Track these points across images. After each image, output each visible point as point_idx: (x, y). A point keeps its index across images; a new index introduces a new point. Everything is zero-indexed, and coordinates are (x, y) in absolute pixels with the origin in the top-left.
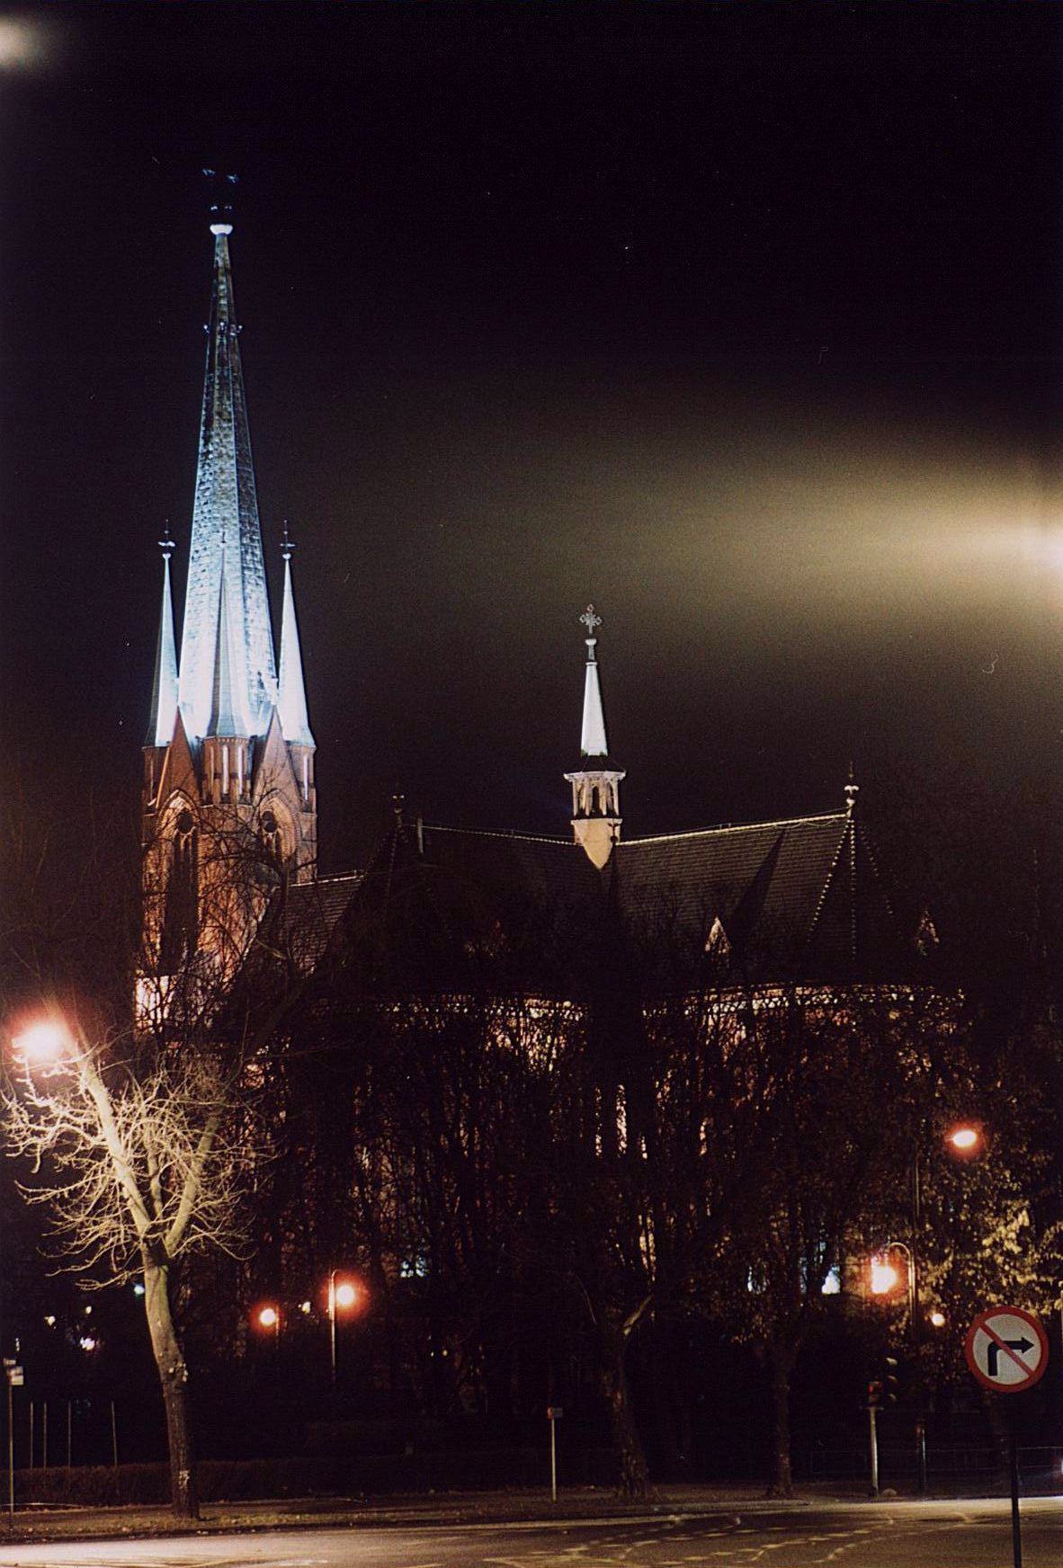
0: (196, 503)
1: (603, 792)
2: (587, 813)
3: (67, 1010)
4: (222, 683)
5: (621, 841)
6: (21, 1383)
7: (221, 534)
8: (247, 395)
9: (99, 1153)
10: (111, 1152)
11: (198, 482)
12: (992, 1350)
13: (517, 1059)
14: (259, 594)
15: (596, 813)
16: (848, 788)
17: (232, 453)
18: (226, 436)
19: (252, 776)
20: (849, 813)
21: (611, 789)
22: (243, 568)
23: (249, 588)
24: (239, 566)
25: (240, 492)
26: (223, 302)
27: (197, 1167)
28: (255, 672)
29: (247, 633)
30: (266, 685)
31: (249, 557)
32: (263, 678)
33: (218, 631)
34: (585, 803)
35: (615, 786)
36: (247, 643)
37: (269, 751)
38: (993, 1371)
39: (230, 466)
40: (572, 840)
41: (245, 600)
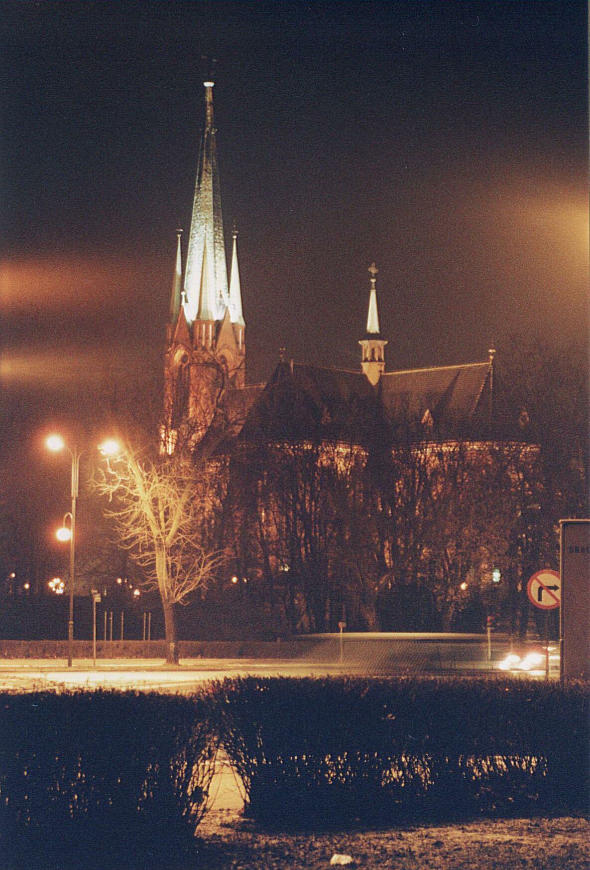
0: (194, 211)
1: (376, 350)
2: (369, 360)
3: (123, 435)
4: (203, 295)
6: (100, 601)
7: (204, 226)
8: (218, 160)
9: (136, 499)
11: (195, 202)
12: (540, 589)
13: (331, 470)
14: (221, 254)
15: (373, 360)
16: (491, 351)
17: (211, 189)
18: (208, 181)
19: (216, 338)
20: (491, 363)
21: (380, 349)
22: (215, 242)
23: (217, 252)
24: (212, 241)
25: (214, 207)
26: (209, 118)
27: (180, 507)
28: (218, 290)
29: (215, 273)
30: (223, 296)
31: (217, 237)
32: (222, 293)
33: (202, 271)
34: (368, 355)
35: (382, 348)
36: (215, 277)
37: (224, 327)
38: (540, 599)
39: (210, 194)
40: (362, 372)
41: (215, 256)
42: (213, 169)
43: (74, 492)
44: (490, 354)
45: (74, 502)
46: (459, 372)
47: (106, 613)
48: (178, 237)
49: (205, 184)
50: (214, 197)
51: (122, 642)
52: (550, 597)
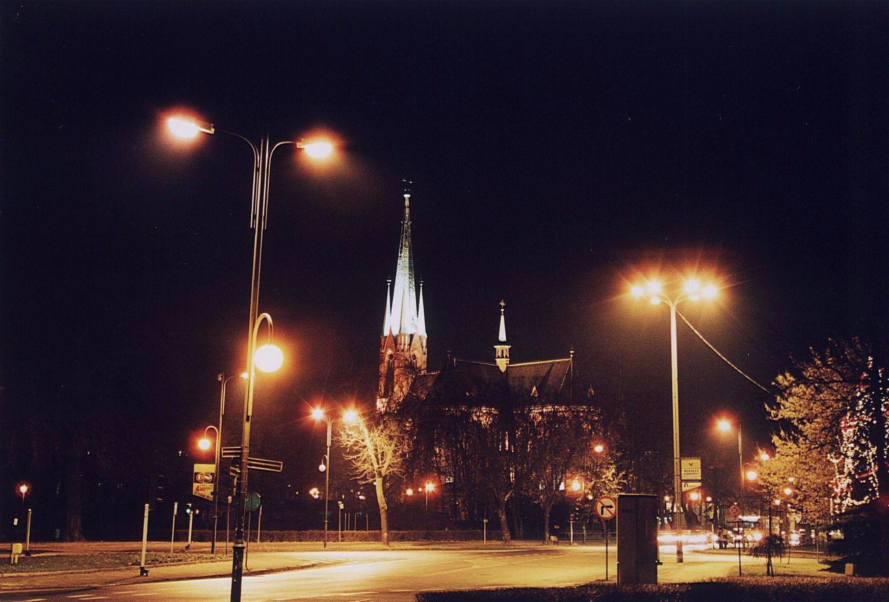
1: (505, 351)
12: (602, 508)
14: (414, 294)
15: (503, 357)
16: (571, 352)
20: (571, 359)
27: (391, 452)
31: (411, 285)
34: (500, 354)
35: (508, 350)
38: (602, 513)
42: (409, 245)
43: (329, 443)
44: (571, 354)
45: (328, 449)
46: (553, 363)
47: (262, 141)
48: (388, 285)
49: (405, 254)
50: (409, 261)
51: (355, 531)
52: (607, 511)
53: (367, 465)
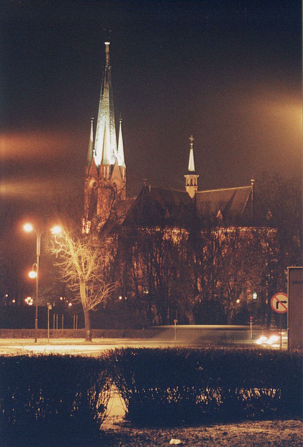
0: (99, 108)
1: (193, 180)
2: (190, 185)
3: (63, 224)
4: (104, 152)
5: (198, 191)
6: (51, 309)
7: (105, 116)
8: (112, 82)
9: (70, 256)
10: (73, 256)
11: (100, 104)
12: (278, 303)
13: (170, 241)
14: (114, 130)
15: (191, 185)
16: (252, 180)
17: (108, 97)
18: (107, 93)
19: (111, 174)
20: (252, 186)
21: (195, 179)
22: (110, 124)
23: (111, 129)
24: (109, 124)
25: (110, 106)
26: (107, 61)
27: (93, 260)
28: (112, 149)
29: (111, 140)
30: (115, 152)
31: (111, 122)
32: (114, 151)
33: (104, 139)
34: (189, 182)
35: (196, 179)
36: (111, 142)
37: (115, 168)
38: (277, 308)
39: (108, 100)
40: (186, 191)
41: (110, 132)
42: (110, 87)
43: (38, 253)
44: (252, 182)
45: (38, 258)
46: (236, 191)
47: (54, 315)
48: (91, 122)
49: (105, 94)
50: (110, 101)
51: (62, 330)
52: (282, 307)
53: (71, 272)
